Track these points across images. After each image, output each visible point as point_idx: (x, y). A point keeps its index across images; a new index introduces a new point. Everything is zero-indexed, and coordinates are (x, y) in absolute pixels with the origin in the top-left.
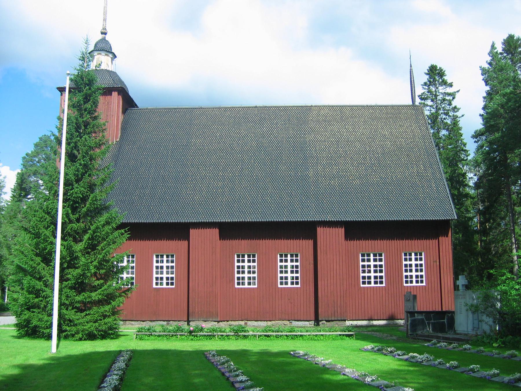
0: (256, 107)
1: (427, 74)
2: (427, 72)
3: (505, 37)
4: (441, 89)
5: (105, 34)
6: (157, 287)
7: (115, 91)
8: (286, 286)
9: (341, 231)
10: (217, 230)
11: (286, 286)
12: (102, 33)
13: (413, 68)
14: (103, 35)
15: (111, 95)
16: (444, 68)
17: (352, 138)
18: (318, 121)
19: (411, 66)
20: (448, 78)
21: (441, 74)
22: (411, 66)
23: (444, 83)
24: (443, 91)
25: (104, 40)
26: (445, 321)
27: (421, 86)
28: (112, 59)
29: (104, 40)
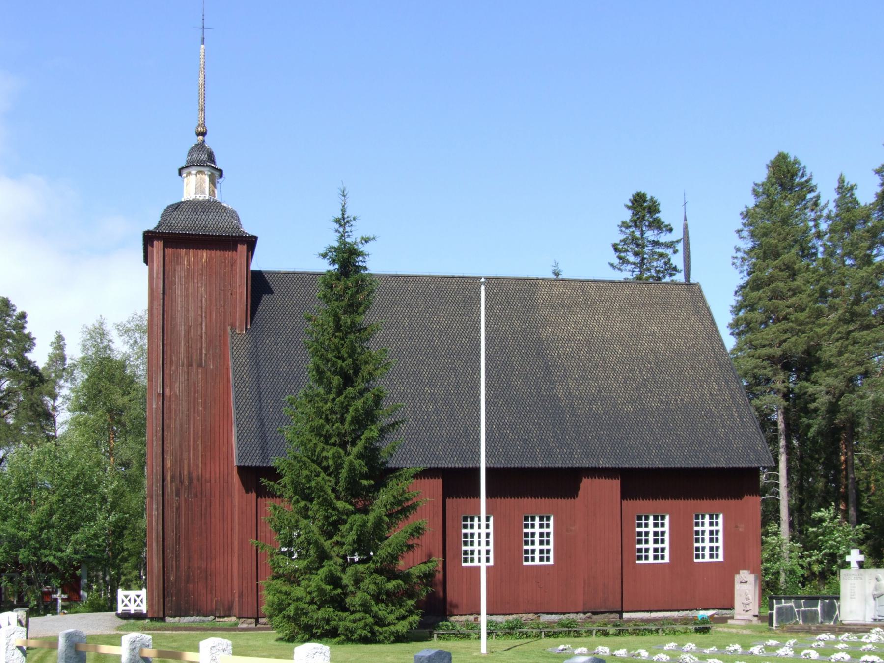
0: (453, 277)
1: (629, 208)
2: (630, 204)
3: (773, 156)
4: (650, 235)
5: (203, 134)
6: (542, 563)
7: (242, 243)
8: (646, 562)
9: (615, 484)
10: (440, 481)
11: (646, 562)
12: (199, 134)
13: (688, 222)
14: (201, 137)
15: (235, 249)
16: (658, 198)
17: (608, 335)
18: (552, 307)
19: (685, 220)
20: (664, 216)
21: (654, 208)
22: (685, 220)
23: (657, 225)
24: (651, 238)
25: (201, 147)
26: (819, 608)
27: (618, 229)
28: (213, 182)
29: (201, 147)
